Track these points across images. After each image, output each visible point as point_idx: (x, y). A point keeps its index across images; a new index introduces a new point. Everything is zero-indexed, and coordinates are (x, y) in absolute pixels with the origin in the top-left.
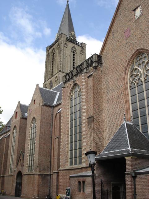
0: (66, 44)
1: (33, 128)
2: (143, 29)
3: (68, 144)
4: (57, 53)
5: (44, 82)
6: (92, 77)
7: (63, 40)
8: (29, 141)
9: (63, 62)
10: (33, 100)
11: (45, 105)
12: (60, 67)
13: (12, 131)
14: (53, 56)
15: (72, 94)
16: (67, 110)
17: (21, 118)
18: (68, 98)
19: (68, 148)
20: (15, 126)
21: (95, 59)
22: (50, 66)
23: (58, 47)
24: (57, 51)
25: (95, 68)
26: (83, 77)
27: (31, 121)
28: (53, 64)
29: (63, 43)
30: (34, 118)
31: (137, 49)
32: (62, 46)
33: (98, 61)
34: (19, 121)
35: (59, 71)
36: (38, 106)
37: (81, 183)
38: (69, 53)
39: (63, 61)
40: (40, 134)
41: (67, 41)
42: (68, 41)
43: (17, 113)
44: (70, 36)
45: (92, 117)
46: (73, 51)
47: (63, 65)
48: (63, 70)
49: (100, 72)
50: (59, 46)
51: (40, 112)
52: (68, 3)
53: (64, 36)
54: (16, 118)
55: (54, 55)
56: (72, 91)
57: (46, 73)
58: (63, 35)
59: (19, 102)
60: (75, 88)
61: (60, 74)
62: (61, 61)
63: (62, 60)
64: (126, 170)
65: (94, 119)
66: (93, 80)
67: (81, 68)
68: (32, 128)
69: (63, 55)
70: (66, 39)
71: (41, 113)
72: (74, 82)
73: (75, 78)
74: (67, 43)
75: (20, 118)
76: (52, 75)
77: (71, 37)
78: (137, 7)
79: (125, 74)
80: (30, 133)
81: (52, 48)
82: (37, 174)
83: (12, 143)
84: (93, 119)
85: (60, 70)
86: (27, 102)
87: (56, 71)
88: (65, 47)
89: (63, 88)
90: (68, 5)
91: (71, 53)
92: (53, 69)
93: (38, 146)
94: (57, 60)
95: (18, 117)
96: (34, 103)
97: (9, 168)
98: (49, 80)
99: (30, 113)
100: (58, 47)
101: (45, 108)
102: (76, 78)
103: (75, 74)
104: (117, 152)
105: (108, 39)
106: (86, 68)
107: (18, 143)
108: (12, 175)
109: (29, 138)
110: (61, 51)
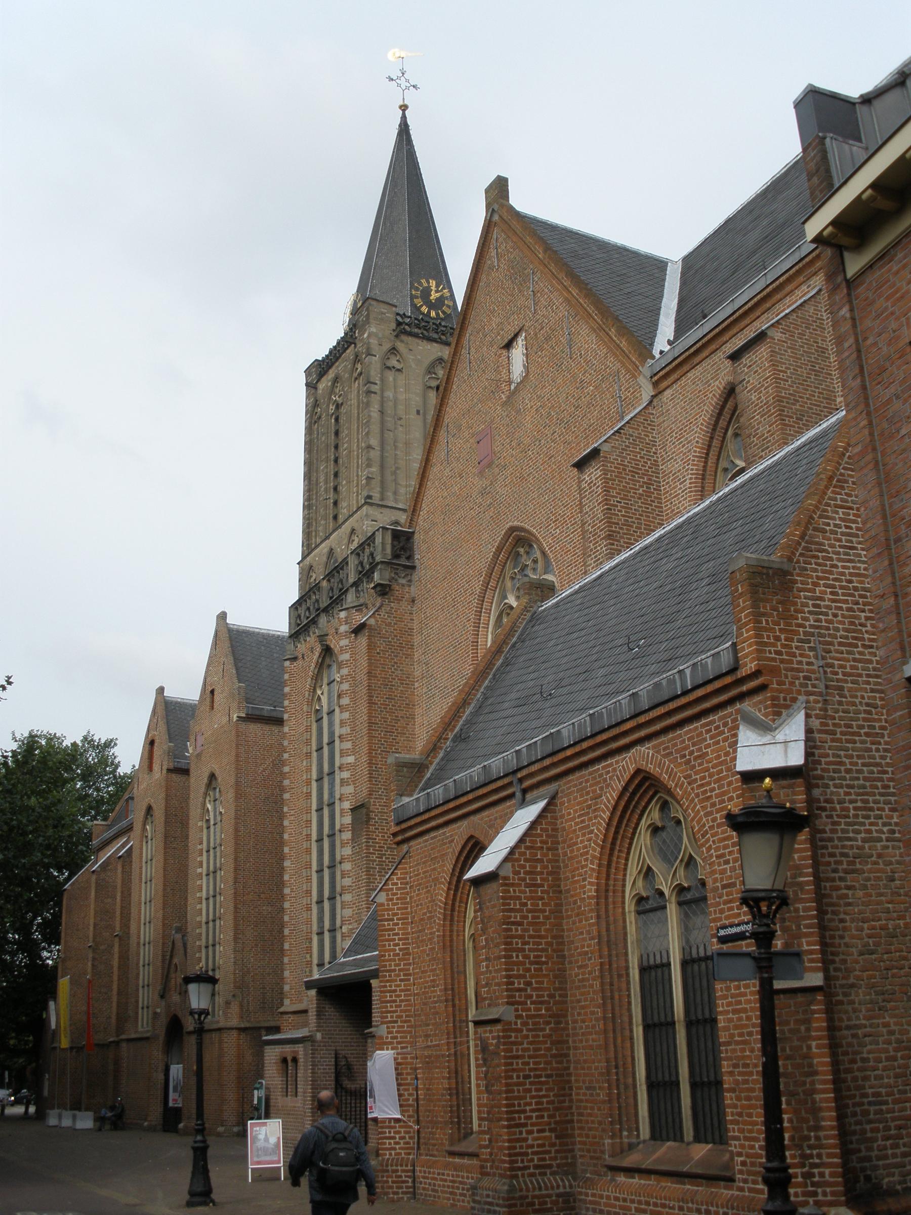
0: (393, 350)
1: (212, 822)
2: (527, 441)
3: (309, 909)
4: (354, 402)
5: (304, 557)
6: (366, 632)
7: (378, 333)
8: (199, 883)
9: (382, 449)
10: (208, 692)
11: (252, 718)
12: (368, 478)
13: (137, 827)
14: (337, 420)
15: (319, 692)
16: (305, 764)
17: (169, 770)
18: (305, 708)
19: (309, 922)
20: (149, 809)
21: (383, 548)
22: (325, 468)
23: (354, 369)
24: (354, 394)
25: (383, 590)
26: (343, 628)
27: (203, 789)
28: (336, 461)
29: (379, 351)
30: (212, 776)
31: (508, 526)
32: (375, 363)
33: (396, 556)
34: (163, 784)
35: (366, 503)
36: (225, 720)
37: (289, 1061)
38: (416, 400)
39: (382, 443)
40: (236, 851)
41: (397, 336)
42: (404, 337)
43: (152, 743)
44: (419, 302)
45: (362, 806)
46: (434, 384)
47: (382, 467)
48: (382, 493)
49: (404, 604)
50: (359, 366)
51: (233, 754)
52: (404, 117)
53: (383, 308)
54: (151, 768)
55: (343, 410)
56: (317, 677)
57: (308, 506)
58: (376, 308)
59: (222, 616)
60: (329, 666)
61: (367, 515)
62: (369, 447)
63: (374, 442)
64: (371, 1022)
65: (372, 815)
66: (371, 647)
67: (372, 554)
68: (208, 821)
69: (382, 412)
70: (393, 325)
71: (237, 756)
72: (322, 638)
73: (323, 620)
74: (400, 346)
75: (165, 767)
76: (335, 517)
77: (425, 309)
78: (516, 336)
79: (477, 626)
80: (201, 843)
81: (331, 374)
82: (232, 1029)
83: (143, 885)
84: (368, 815)
85: (369, 497)
86: (187, 688)
87: (350, 499)
88: (389, 368)
89: (287, 663)
90: (404, 131)
91: (425, 397)
92: (340, 488)
93: (232, 908)
94: (351, 443)
95: (156, 767)
96: (212, 707)
97: (137, 1002)
98: (324, 548)
99: (199, 750)
100: (354, 369)
101: (255, 729)
102: (328, 622)
103: (325, 605)
104: (672, 927)
105: (434, 460)
106: (356, 584)
107: (164, 890)
108: (148, 1035)
109: (199, 870)
110: (369, 392)
